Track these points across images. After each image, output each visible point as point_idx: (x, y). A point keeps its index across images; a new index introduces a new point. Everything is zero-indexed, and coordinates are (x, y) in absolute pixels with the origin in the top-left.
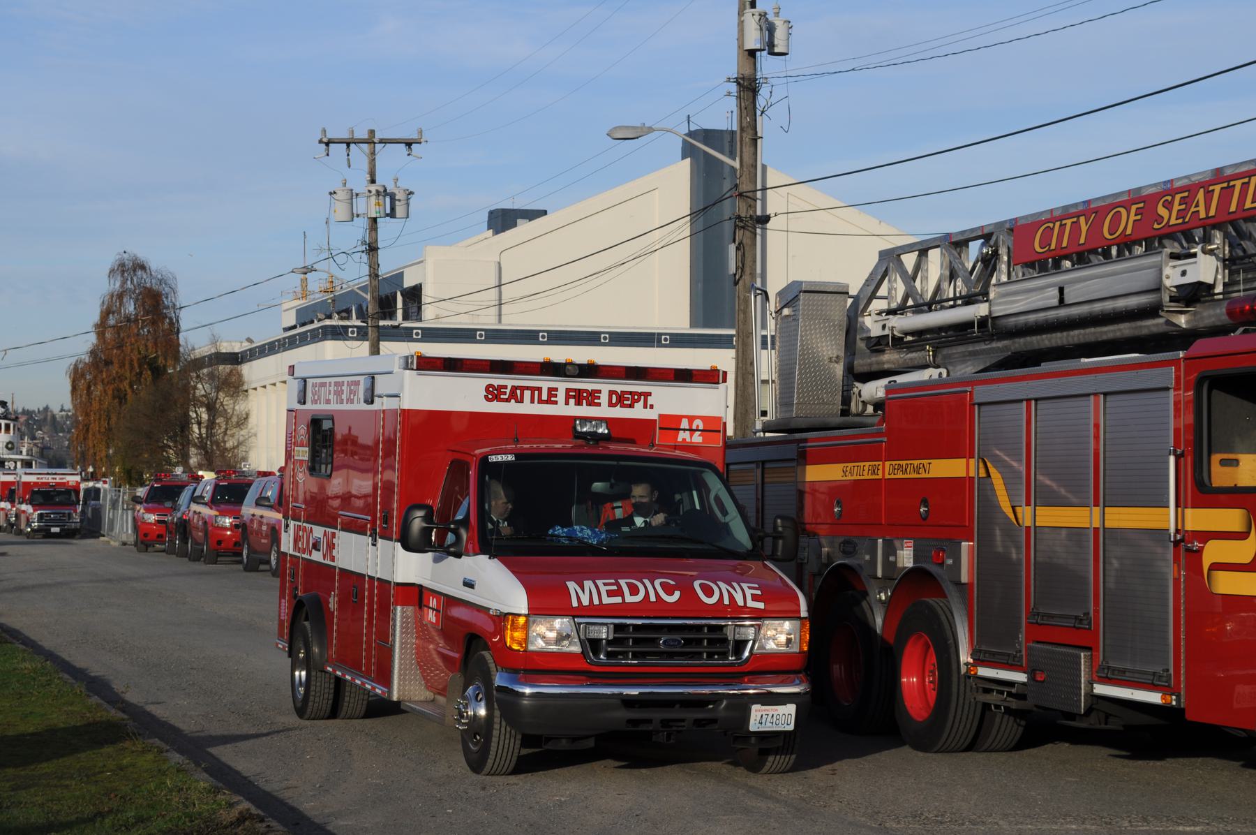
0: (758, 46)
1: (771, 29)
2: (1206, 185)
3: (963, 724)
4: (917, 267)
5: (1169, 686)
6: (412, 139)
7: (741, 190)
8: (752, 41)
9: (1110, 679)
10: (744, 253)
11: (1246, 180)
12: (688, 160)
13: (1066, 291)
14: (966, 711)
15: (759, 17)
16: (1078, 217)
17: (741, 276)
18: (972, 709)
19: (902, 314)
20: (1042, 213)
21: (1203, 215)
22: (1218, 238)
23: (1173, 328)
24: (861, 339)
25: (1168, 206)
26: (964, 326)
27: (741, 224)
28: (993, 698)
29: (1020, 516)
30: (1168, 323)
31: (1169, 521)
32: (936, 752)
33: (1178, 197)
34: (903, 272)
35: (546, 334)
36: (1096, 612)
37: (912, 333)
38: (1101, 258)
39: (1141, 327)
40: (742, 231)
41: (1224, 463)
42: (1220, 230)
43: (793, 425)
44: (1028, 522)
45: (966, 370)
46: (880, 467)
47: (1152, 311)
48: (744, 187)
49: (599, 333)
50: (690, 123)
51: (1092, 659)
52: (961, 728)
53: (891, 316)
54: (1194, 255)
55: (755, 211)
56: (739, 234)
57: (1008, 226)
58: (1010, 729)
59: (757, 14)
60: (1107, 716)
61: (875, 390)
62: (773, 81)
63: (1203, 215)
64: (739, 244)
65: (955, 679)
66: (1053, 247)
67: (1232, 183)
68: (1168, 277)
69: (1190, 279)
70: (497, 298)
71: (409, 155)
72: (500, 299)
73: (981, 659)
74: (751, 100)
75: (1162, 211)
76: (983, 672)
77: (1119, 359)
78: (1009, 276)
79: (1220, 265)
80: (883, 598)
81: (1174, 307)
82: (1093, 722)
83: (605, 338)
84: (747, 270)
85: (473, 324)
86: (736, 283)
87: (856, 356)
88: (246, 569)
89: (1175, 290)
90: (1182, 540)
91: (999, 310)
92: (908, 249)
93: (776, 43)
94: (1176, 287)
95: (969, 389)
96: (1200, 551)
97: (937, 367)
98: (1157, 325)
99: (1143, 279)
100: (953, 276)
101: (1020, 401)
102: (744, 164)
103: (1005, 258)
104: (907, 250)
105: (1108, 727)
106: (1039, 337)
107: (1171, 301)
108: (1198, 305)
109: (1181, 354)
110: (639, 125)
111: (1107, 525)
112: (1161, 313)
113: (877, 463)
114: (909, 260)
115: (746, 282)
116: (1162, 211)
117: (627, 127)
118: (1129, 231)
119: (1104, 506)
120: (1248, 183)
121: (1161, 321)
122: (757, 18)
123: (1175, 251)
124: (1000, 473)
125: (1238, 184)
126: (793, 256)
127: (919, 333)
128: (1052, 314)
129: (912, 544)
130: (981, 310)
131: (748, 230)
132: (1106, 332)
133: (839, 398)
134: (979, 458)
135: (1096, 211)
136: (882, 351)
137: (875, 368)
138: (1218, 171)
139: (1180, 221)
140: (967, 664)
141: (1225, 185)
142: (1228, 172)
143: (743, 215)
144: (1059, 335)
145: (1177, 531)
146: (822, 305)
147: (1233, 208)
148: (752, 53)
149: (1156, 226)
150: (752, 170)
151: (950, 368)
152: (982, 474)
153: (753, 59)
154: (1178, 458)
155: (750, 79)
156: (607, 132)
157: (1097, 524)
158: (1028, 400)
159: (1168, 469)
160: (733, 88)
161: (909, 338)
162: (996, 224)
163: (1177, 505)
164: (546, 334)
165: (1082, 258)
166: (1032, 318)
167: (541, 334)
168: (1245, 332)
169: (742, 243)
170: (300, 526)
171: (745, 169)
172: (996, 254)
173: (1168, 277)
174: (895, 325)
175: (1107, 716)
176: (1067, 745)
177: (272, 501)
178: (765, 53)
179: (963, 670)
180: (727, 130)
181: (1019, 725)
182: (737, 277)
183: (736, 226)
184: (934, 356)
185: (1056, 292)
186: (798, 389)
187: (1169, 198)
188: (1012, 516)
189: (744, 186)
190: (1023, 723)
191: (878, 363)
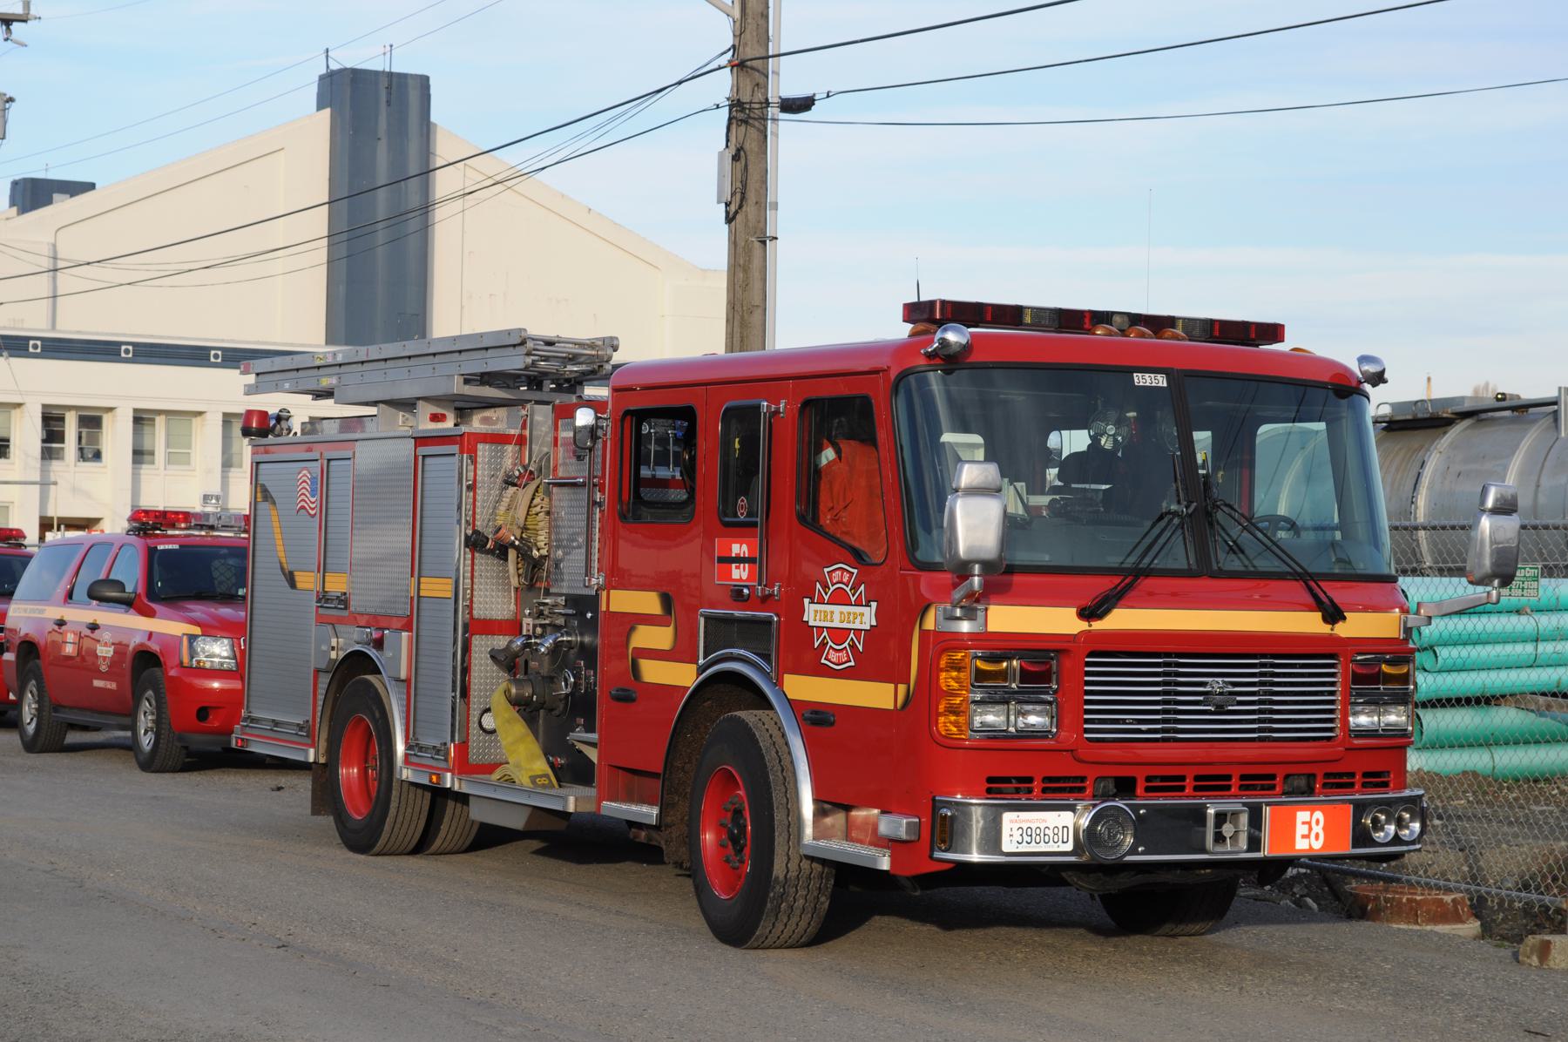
6: (13, 14)
10: (746, 166)
12: (327, 112)
17: (741, 207)
27: (741, 116)
35: (130, 348)
40: (743, 128)
49: (209, 349)
50: (329, 59)
64: (738, 150)
71: (6, 40)
83: (216, 356)
84: (752, 196)
85: (14, 329)
88: (32, 746)
115: (750, 217)
126: (470, 252)
131: (754, 126)
150: (761, 22)
164: (130, 348)
167: (123, 348)
169: (742, 148)
171: (749, 21)
177: (129, 588)
180: (384, 72)
189: (748, 49)
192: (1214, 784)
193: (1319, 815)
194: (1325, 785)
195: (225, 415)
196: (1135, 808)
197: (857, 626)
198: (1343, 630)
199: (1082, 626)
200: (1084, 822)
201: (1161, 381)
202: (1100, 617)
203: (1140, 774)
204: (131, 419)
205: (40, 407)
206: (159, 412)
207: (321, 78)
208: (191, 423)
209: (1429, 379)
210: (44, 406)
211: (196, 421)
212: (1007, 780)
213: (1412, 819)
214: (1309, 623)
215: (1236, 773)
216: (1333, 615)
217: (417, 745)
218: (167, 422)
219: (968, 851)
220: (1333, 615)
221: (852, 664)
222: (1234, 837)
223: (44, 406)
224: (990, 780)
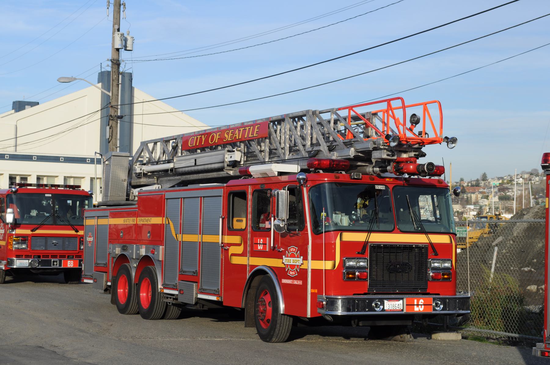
0: (120, 47)
1: (126, 40)
2: (238, 128)
3: (159, 309)
4: (153, 149)
5: (219, 294)
7: (112, 105)
8: (118, 45)
9: (203, 292)
11: (250, 127)
13: (197, 161)
14: (160, 305)
15: (120, 36)
16: (202, 135)
17: (111, 140)
18: (163, 304)
19: (147, 165)
20: (192, 133)
21: (237, 138)
22: (242, 145)
23: (229, 175)
24: (134, 173)
25: (228, 134)
26: (166, 171)
27: (112, 118)
28: (169, 300)
29: (178, 237)
30: (227, 173)
31: (219, 240)
32: (150, 319)
33: (231, 131)
34: (148, 150)
36: (199, 270)
37: (151, 172)
38: (209, 150)
39: (220, 174)
40: (112, 121)
41: (237, 221)
42: (243, 143)
43: (108, 204)
44: (180, 240)
45: (167, 186)
46: (136, 220)
47: (221, 169)
48: (113, 104)
49: (60, 157)
51: (198, 286)
52: (159, 311)
53: (143, 166)
54: (234, 151)
55: (117, 114)
56: (111, 122)
57: (181, 136)
58: (175, 311)
59: (120, 34)
60: (203, 305)
61: (136, 192)
62: (126, 61)
63: (237, 138)
64: (111, 126)
65: (157, 293)
66: (194, 145)
67: (246, 128)
68: (226, 158)
69: (232, 159)
70: (15, 143)
72: (16, 144)
73: (165, 286)
74: (117, 68)
75: (226, 136)
76: (166, 291)
77: (206, 186)
78: (182, 154)
79: (243, 155)
80: (135, 266)
81: (229, 168)
82: (198, 307)
84: (114, 137)
86: (109, 142)
87: (132, 179)
89: (228, 162)
90: (223, 246)
91: (177, 166)
92: (150, 142)
93: (128, 46)
94: (229, 161)
95: (164, 193)
96: (228, 250)
97: (158, 184)
98: (224, 174)
99: (219, 159)
100: (164, 152)
101: (179, 198)
102: (113, 94)
103: (180, 148)
104: (149, 142)
105: (203, 309)
106: (189, 176)
107: (227, 166)
108: (236, 168)
109: (225, 185)
110: (71, 77)
111: (203, 241)
112: (224, 170)
113: (135, 218)
114: (151, 146)
116: (226, 136)
117: (65, 78)
118: (216, 142)
119: (202, 235)
120: (250, 128)
121: (225, 172)
122: (120, 36)
123: (229, 149)
124: (172, 222)
125: (247, 128)
127: (153, 172)
128: (193, 168)
129: (145, 247)
130: (171, 165)
132: (209, 175)
133: (125, 194)
134: (166, 217)
135: (207, 134)
136: (141, 178)
137: (138, 184)
138: (243, 123)
139: (231, 139)
140: (161, 288)
141: (244, 128)
142: (245, 124)
143: (112, 115)
144: (195, 175)
145: (222, 243)
146: (120, 161)
147: (246, 137)
148: (118, 50)
149: (224, 141)
150: (117, 97)
151: (162, 185)
152: (167, 223)
153: (118, 52)
154: (223, 219)
155: (116, 60)
156: (57, 79)
157: (200, 240)
158: (181, 198)
159: (219, 222)
160: (110, 63)
161: (149, 174)
162: (178, 135)
163: (222, 234)
165: (203, 149)
166: (187, 169)
168: (245, 178)
170: (317, 257)
172: (177, 146)
173: (226, 158)
174: (144, 169)
175: (203, 305)
176: (198, 318)
178: (123, 50)
179: (159, 290)
181: (179, 310)
182: (110, 140)
183: (110, 119)
184: (157, 180)
185: (194, 161)
186: (110, 191)
187: (228, 131)
188: (175, 237)
189: (113, 103)
190: (181, 309)
191: (139, 182)
192: (54, 256)
193: (72, 261)
194: (75, 257)
195: (65, 177)
196: (39, 260)
197: (298, 264)
198: (78, 233)
199: (32, 233)
200: (30, 261)
201: (50, 195)
202: (34, 231)
203: (41, 255)
204: (36, 178)
205: (8, 175)
206: (45, 176)
207: (99, 73)
208: (81, 181)
209: (451, 164)
210: (10, 174)
211: (82, 180)
212: (20, 255)
213: (441, 304)
214: (73, 232)
215: (67, 255)
216: (77, 231)
217: (202, 289)
218: (47, 179)
219: (14, 266)
220: (77, 231)
221: (297, 275)
222: (56, 265)
223: (10, 174)
224: (16, 255)
